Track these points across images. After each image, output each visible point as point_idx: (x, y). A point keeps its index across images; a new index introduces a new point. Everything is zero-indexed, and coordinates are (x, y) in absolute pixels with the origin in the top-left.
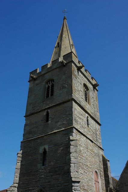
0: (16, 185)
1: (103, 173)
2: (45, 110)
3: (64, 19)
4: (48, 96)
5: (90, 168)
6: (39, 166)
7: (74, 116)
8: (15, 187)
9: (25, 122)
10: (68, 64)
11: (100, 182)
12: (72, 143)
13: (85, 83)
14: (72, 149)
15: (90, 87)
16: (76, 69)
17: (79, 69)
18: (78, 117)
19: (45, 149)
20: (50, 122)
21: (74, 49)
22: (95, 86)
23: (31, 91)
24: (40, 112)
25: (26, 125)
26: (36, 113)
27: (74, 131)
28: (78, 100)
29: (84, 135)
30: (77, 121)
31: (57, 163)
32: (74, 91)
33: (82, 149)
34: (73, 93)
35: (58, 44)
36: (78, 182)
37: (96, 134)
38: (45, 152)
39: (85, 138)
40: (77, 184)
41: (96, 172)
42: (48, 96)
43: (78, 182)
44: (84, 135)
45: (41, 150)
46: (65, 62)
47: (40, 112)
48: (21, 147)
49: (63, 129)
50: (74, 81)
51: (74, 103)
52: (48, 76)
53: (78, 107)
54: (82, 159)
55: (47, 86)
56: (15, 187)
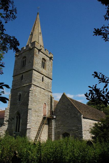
0: (9, 109)
1: (49, 104)
2: (21, 74)
3: (38, 14)
4: (23, 66)
5: (41, 102)
6: (18, 101)
7: (33, 78)
8: (8, 110)
9: (13, 79)
10: (33, 49)
11: (47, 108)
12: (30, 92)
13: (44, 57)
14: (30, 94)
15: (48, 59)
16: (37, 51)
17: (39, 50)
18: (36, 78)
19: (20, 94)
20: (23, 80)
21: (41, 35)
22: (51, 58)
23: (16, 62)
24: (19, 74)
25: (13, 81)
26: (17, 75)
27: (32, 85)
28: (37, 69)
29: (39, 87)
30: (35, 81)
32: (34, 64)
33: (36, 94)
34: (34, 65)
35: (32, 32)
36: (31, 109)
37: (48, 85)
38: (20, 95)
39: (39, 88)
40: (30, 110)
41: (45, 103)
42: (23, 66)
43: (31, 109)
44: (39, 87)
45: (19, 94)
46: (31, 47)
47: (19, 74)
48: (11, 92)
49: (28, 84)
50: (35, 59)
51: (34, 71)
52: (24, 55)
53: (37, 72)
54: (36, 98)
55: (23, 60)
56: (8, 110)
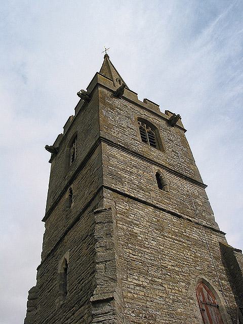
5: (177, 273)
31: (81, 281)
